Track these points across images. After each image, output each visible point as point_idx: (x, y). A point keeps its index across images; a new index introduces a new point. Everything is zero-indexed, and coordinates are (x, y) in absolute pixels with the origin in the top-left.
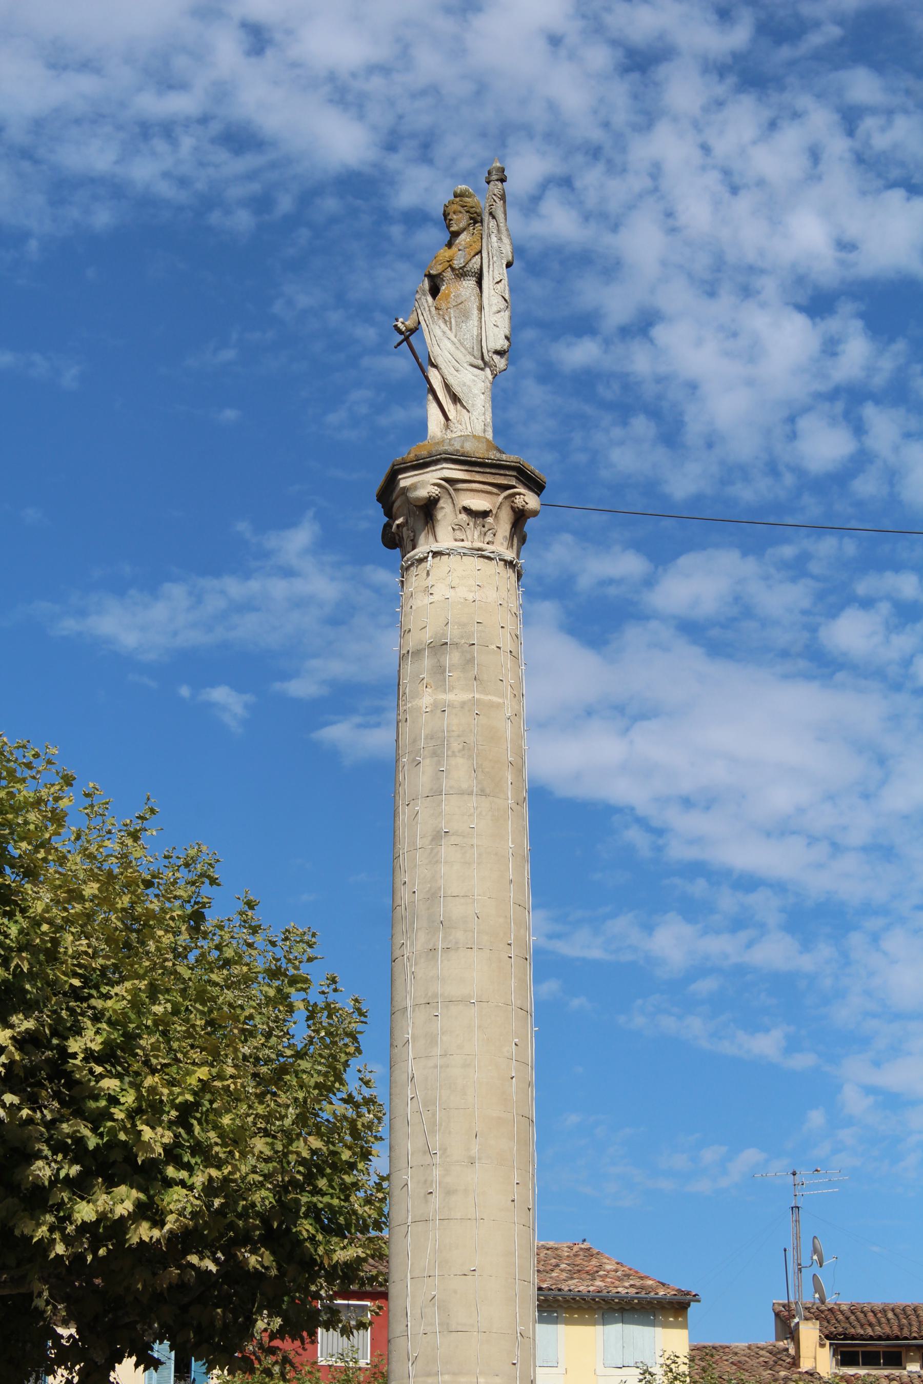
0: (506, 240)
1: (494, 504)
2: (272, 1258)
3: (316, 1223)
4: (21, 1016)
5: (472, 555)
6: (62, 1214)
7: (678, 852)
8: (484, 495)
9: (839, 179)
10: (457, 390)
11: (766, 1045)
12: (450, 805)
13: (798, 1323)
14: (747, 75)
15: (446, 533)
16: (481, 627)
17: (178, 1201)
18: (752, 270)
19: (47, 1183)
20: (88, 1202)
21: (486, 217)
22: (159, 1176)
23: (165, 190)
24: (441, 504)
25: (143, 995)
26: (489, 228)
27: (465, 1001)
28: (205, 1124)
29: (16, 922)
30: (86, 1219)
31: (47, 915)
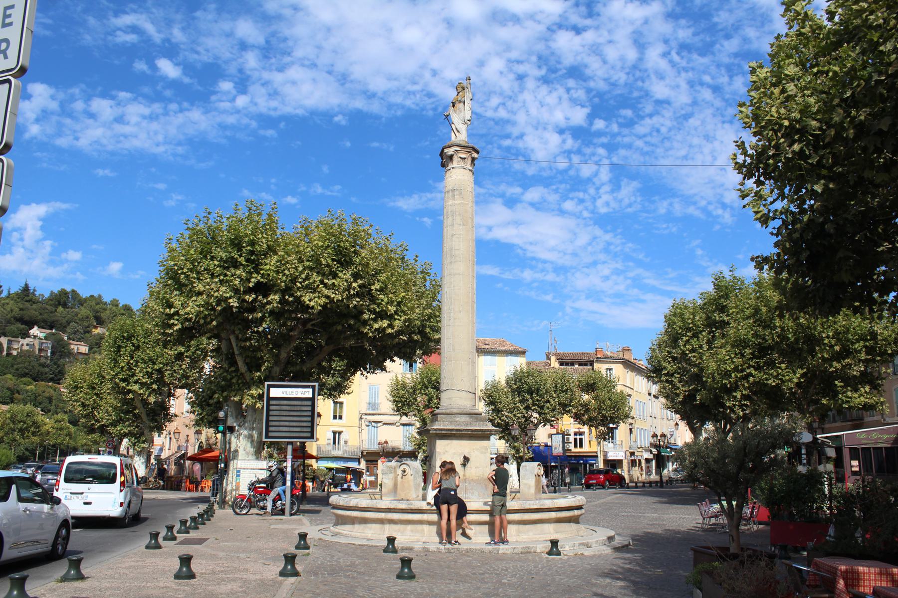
7: (529, 255)
9: (566, 104)
11: (549, 298)
14: (545, 80)
15: (456, 162)
18: (546, 124)
23: (413, 106)
27: (459, 274)
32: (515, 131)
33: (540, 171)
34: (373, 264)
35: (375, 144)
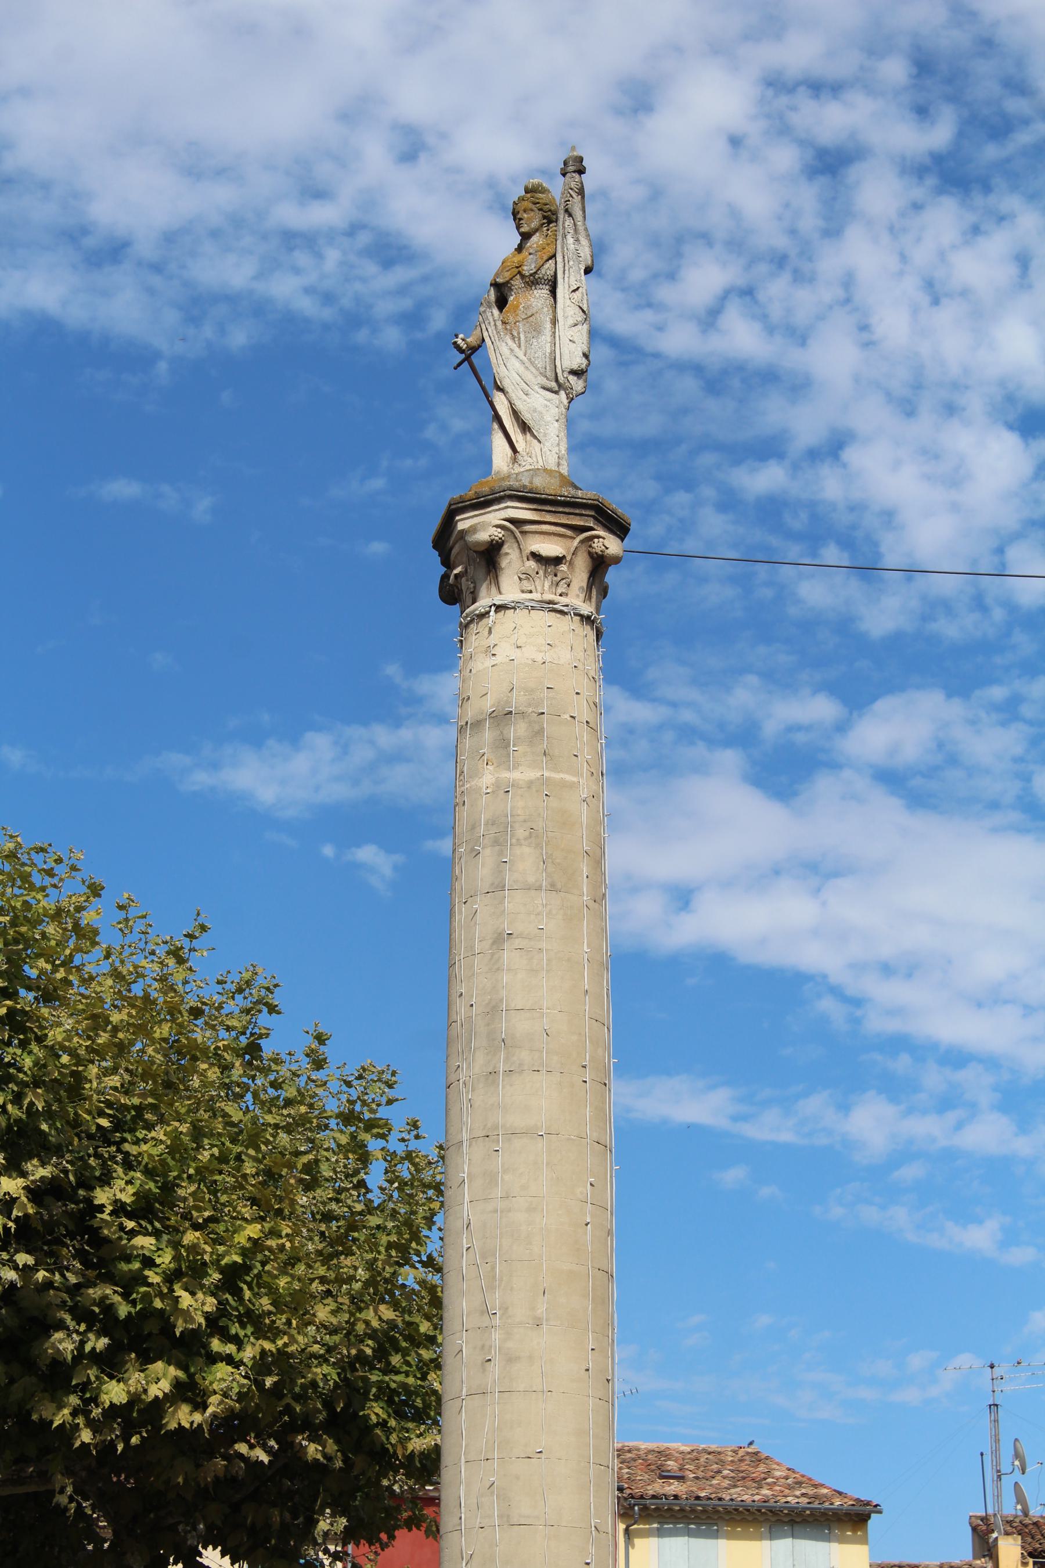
0: (584, 242)
1: (568, 549)
2: (336, 1448)
3: (389, 1406)
4: (35, 1162)
5: (542, 609)
6: (88, 1395)
7: (876, 1024)
8: (556, 538)
10: (526, 416)
11: (980, 1237)
12: (513, 902)
13: (997, 1538)
14: (950, 175)
16: (551, 693)
17: (223, 1379)
18: (956, 386)
19: (69, 1357)
20: (119, 1381)
21: (561, 215)
22: (203, 1351)
23: (307, 306)
24: (506, 549)
25: (186, 1139)
26: (564, 228)
27: (531, 1133)
28: (256, 1290)
29: (30, 1053)
30: (115, 1401)
31: (67, 1044)
32: (807, 425)
33: (925, 618)
34: (103, 1082)
35: (123, 489)
